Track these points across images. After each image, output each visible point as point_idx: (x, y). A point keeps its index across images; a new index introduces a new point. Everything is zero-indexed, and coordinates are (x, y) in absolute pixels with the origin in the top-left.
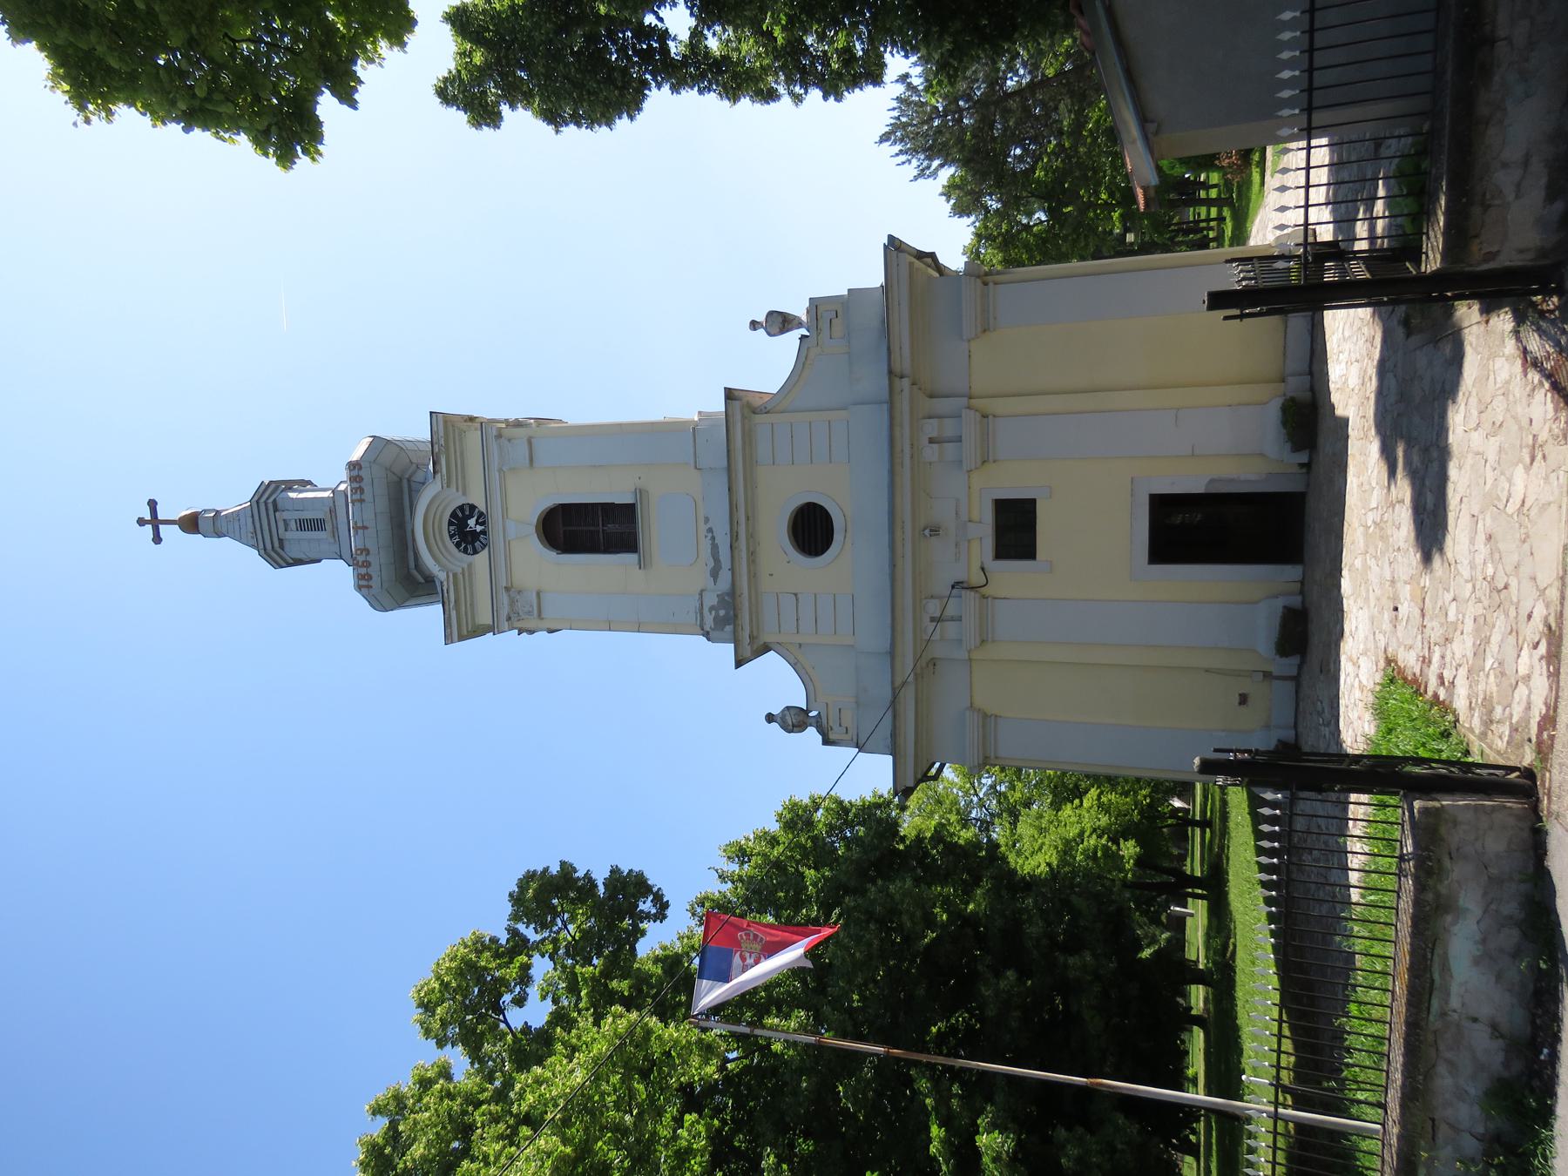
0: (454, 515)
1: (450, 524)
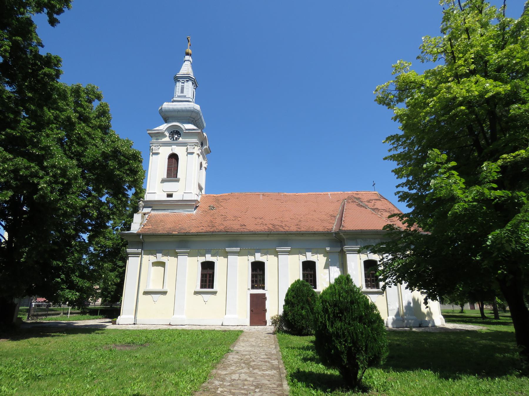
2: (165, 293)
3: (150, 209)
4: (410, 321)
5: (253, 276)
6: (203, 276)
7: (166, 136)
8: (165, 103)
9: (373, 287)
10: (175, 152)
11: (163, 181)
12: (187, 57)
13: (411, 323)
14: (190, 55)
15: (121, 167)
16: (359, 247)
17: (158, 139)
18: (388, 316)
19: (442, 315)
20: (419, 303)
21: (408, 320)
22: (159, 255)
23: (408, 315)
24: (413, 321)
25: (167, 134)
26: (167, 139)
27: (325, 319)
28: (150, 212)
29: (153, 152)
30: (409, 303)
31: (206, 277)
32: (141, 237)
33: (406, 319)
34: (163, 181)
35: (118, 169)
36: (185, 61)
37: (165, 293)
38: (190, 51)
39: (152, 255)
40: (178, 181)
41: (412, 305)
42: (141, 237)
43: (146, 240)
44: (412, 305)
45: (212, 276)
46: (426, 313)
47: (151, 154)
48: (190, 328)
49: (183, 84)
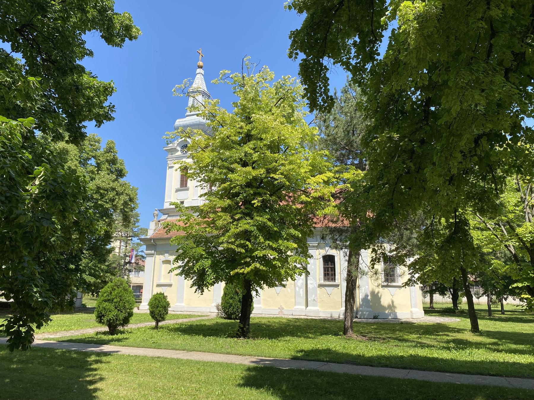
2: (170, 285)
3: (167, 216)
4: (365, 313)
5: (324, 268)
6: (326, 270)
7: (178, 151)
8: (178, 120)
9: (328, 280)
11: (177, 191)
12: (199, 70)
13: (365, 315)
14: (201, 67)
15: (102, 198)
16: (317, 243)
17: (172, 154)
18: (307, 306)
19: (424, 310)
20: (378, 296)
21: (362, 311)
22: (167, 255)
23: (365, 308)
24: (367, 313)
25: (179, 149)
26: (179, 153)
27: (509, 327)
28: (166, 219)
29: (169, 166)
30: (367, 296)
31: (328, 271)
32: (152, 241)
33: (361, 311)
34: (177, 191)
35: (100, 200)
36: (197, 74)
37: (170, 285)
38: (201, 63)
39: (162, 255)
40: (188, 190)
41: (369, 297)
42: (152, 241)
43: (157, 243)
44: (369, 297)
45: (334, 269)
46: (386, 306)
47: (168, 167)
48: (193, 314)
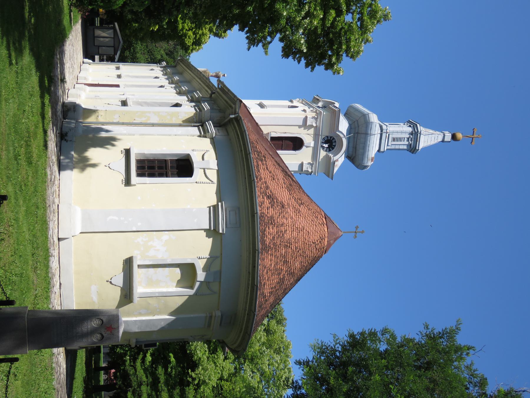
0: (333, 148)
1: (335, 146)
10: (304, 147)
49: (406, 139)
